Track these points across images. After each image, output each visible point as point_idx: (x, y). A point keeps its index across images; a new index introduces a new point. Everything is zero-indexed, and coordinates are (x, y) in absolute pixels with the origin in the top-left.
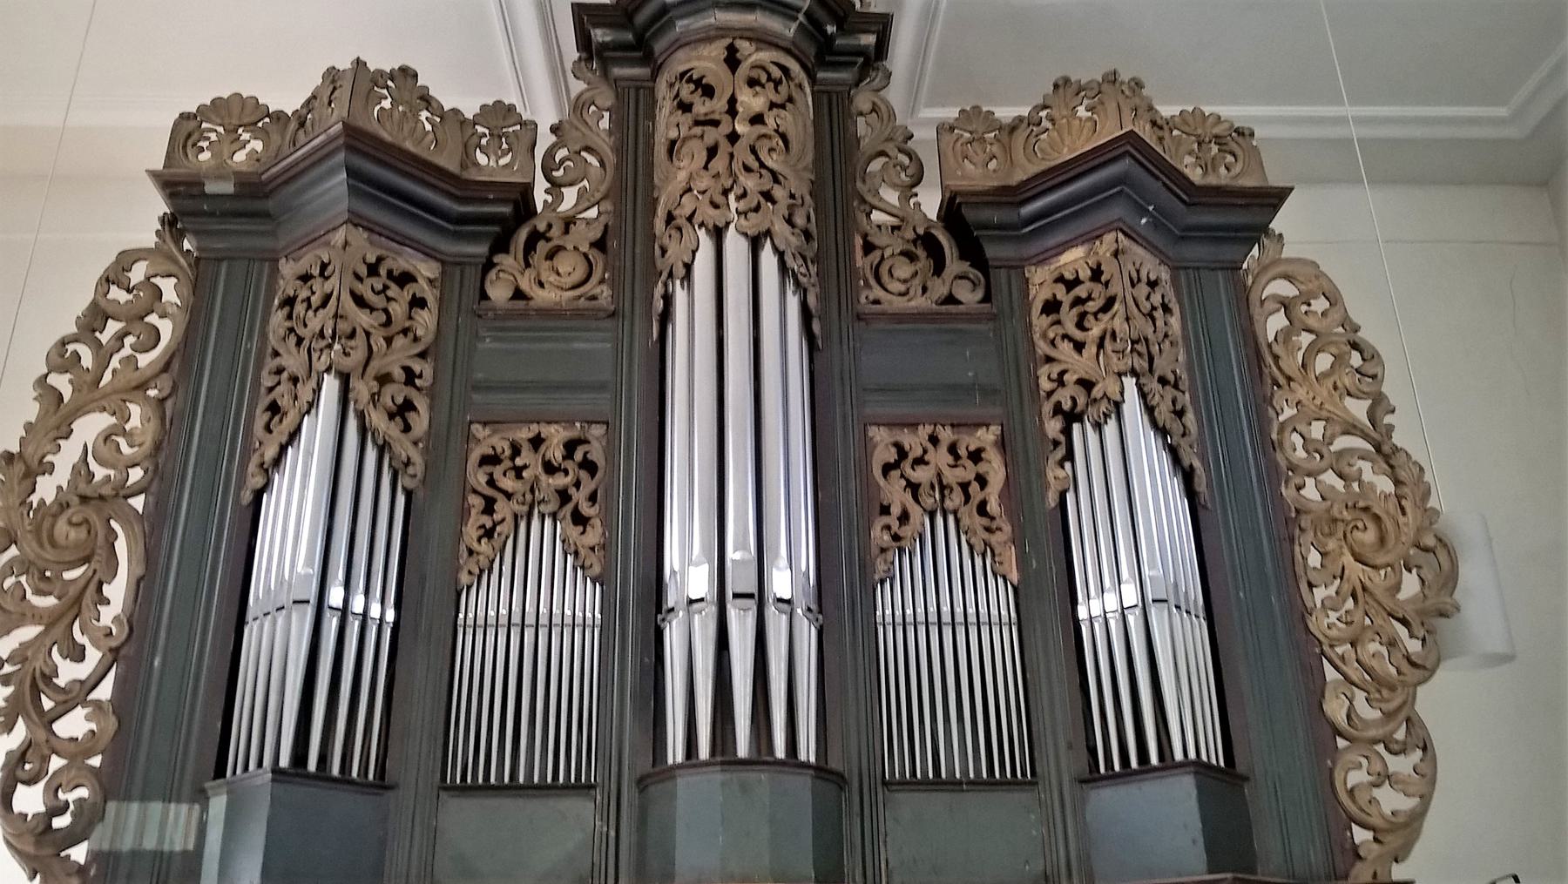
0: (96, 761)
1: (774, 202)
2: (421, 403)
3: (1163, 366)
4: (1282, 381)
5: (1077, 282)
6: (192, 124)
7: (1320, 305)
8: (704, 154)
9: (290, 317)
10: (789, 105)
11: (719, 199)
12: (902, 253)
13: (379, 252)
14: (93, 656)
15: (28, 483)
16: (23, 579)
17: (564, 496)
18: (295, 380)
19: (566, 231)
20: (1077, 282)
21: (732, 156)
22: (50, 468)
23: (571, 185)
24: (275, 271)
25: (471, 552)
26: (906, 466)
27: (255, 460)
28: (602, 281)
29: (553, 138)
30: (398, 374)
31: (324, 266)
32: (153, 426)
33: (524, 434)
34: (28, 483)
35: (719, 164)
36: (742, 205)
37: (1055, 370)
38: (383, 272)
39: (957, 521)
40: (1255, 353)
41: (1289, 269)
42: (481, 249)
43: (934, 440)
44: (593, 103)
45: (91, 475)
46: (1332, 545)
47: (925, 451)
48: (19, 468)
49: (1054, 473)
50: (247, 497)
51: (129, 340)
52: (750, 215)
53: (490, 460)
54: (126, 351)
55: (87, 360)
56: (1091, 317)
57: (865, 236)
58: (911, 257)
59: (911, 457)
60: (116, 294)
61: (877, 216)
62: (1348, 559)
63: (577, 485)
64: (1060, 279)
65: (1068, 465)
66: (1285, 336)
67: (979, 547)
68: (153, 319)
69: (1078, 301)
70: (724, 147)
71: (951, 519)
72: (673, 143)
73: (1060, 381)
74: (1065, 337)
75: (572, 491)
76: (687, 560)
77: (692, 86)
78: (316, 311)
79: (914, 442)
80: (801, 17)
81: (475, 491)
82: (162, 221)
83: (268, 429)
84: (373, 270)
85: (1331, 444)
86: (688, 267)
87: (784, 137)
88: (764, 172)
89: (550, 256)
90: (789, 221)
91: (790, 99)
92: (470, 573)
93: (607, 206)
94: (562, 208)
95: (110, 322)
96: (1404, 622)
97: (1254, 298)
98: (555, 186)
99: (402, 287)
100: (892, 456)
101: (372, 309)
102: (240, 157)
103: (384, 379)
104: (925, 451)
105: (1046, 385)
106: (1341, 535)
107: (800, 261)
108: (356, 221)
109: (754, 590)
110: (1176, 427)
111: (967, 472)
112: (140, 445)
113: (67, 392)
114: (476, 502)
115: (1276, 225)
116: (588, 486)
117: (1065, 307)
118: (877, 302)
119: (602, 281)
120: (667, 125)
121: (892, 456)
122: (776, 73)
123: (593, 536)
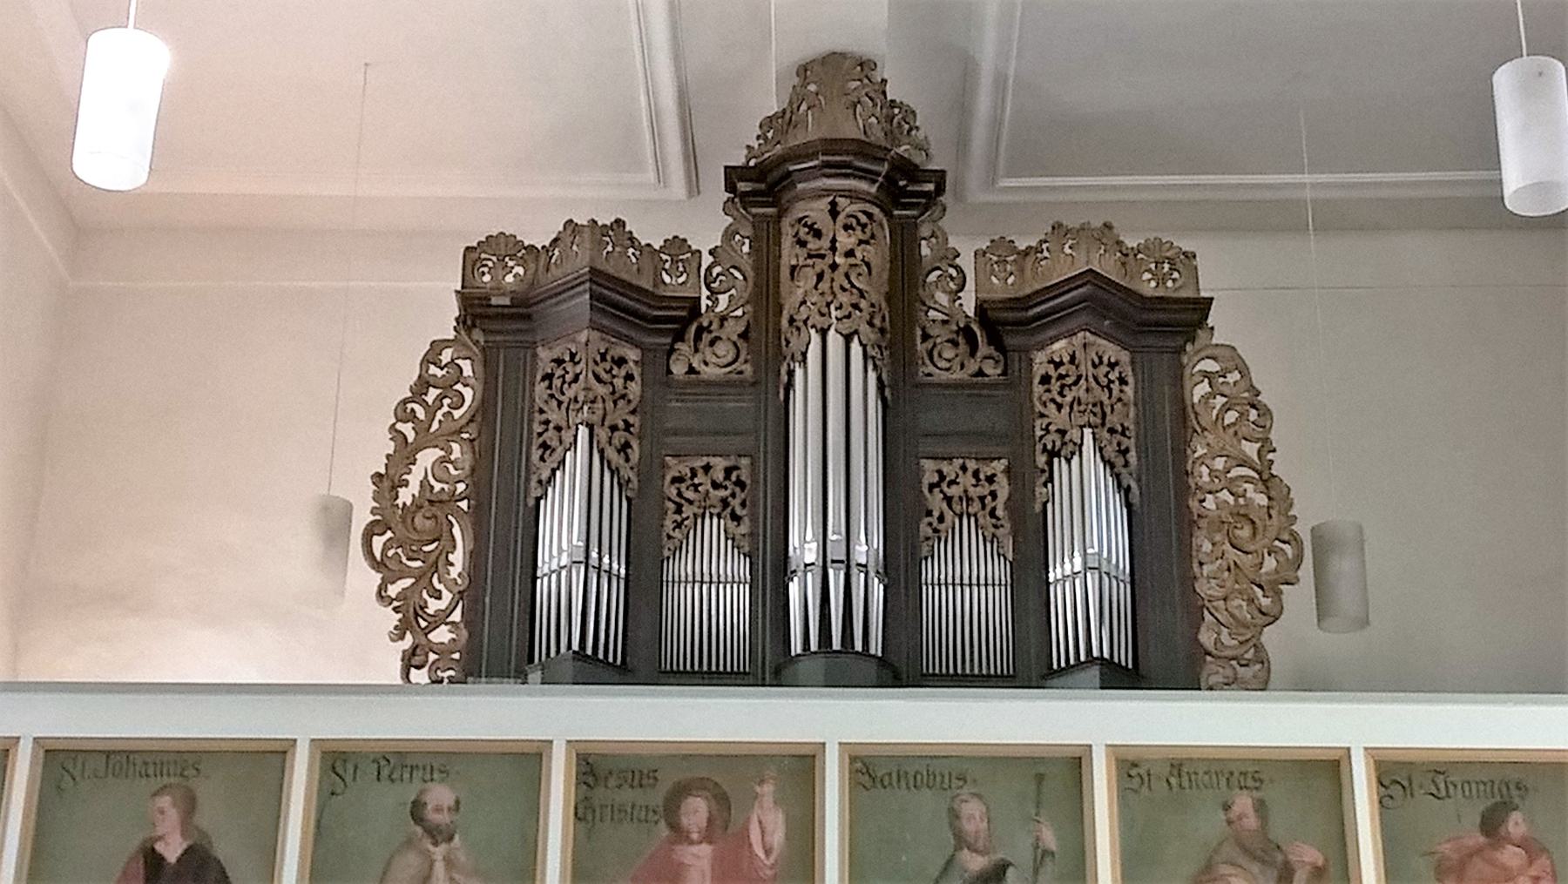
0: (456, 656)
1: (861, 311)
2: (635, 444)
3: (1113, 420)
4: (1199, 430)
5: (1061, 363)
6: (475, 255)
7: (1234, 377)
8: (815, 278)
9: (550, 387)
10: (872, 241)
11: (825, 310)
12: (948, 341)
13: (607, 345)
14: (447, 596)
15: (394, 493)
16: (400, 550)
17: (725, 503)
18: (558, 429)
19: (722, 326)
20: (1061, 363)
21: (833, 280)
22: (406, 484)
23: (724, 293)
24: (535, 355)
25: (669, 537)
26: (944, 486)
27: (534, 479)
28: (746, 362)
29: (711, 259)
30: (621, 425)
31: (573, 356)
32: (468, 456)
33: (699, 463)
34: (394, 493)
35: (825, 286)
36: (839, 314)
37: (1046, 421)
38: (609, 358)
39: (976, 521)
40: (1182, 411)
41: (1216, 352)
42: (669, 340)
43: (964, 468)
44: (738, 233)
45: (432, 487)
46: (1218, 538)
47: (957, 476)
48: (386, 484)
49: (1040, 490)
50: (531, 503)
51: (446, 401)
52: (845, 320)
53: (677, 480)
54: (445, 409)
55: (421, 413)
56: (1067, 388)
57: (923, 329)
58: (955, 344)
59: (948, 479)
60: (433, 370)
61: (932, 313)
62: (1227, 546)
63: (733, 495)
64: (1051, 361)
65: (1050, 485)
66: (1206, 398)
67: (989, 538)
68: (459, 387)
69: (1061, 377)
70: (828, 271)
71: (973, 519)
72: (793, 268)
73: (1047, 430)
74: (1053, 400)
75: (730, 499)
76: (803, 541)
77: (807, 230)
78: (570, 384)
79: (949, 470)
80: (880, 179)
81: (670, 499)
82: (457, 320)
83: (542, 459)
84: (603, 357)
85: (1229, 472)
86: (804, 355)
87: (868, 265)
88: (854, 291)
89: (712, 343)
90: (871, 324)
91: (873, 236)
92: (669, 549)
93: (749, 308)
94: (718, 310)
95: (431, 389)
96: (1260, 586)
97: (1187, 372)
98: (714, 294)
99: (619, 367)
100: (936, 478)
101: (605, 383)
102: (509, 278)
103: (614, 428)
104: (957, 476)
105: (1039, 433)
106: (1225, 532)
107: (877, 350)
108: (595, 326)
109: (843, 558)
110: (1119, 461)
111: (984, 490)
112: (462, 469)
113: (411, 436)
114: (671, 506)
115: (1210, 322)
116: (741, 496)
117: (1053, 381)
118: (929, 375)
119: (746, 362)
120: (789, 254)
121: (936, 478)
122: (864, 219)
123: (744, 528)
